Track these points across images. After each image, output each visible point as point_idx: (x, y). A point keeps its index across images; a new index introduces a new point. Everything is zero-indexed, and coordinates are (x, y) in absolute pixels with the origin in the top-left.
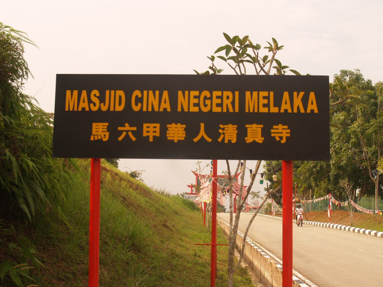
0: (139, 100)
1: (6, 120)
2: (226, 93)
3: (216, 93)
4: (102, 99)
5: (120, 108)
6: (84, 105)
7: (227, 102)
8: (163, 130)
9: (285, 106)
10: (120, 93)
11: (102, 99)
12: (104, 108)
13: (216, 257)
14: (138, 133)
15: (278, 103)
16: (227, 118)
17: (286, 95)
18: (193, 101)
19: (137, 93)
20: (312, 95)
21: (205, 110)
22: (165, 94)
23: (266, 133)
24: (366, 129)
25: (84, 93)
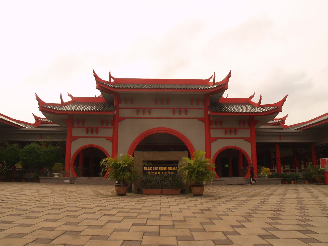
0: (154, 169)
1: (300, 131)
2: (166, 167)
3: (164, 167)
4: (149, 168)
5: (152, 170)
6: (147, 169)
7: (166, 169)
8: (157, 173)
9: (173, 169)
10: (152, 168)
11: (149, 168)
12: (149, 170)
13: (74, 156)
14: (154, 173)
15: (172, 168)
16: (166, 171)
17: (173, 167)
18: (161, 168)
19: (154, 168)
20: (176, 167)
21: (163, 170)
22: (158, 168)
23: (171, 173)
24: (161, 173)
25: (147, 168)
